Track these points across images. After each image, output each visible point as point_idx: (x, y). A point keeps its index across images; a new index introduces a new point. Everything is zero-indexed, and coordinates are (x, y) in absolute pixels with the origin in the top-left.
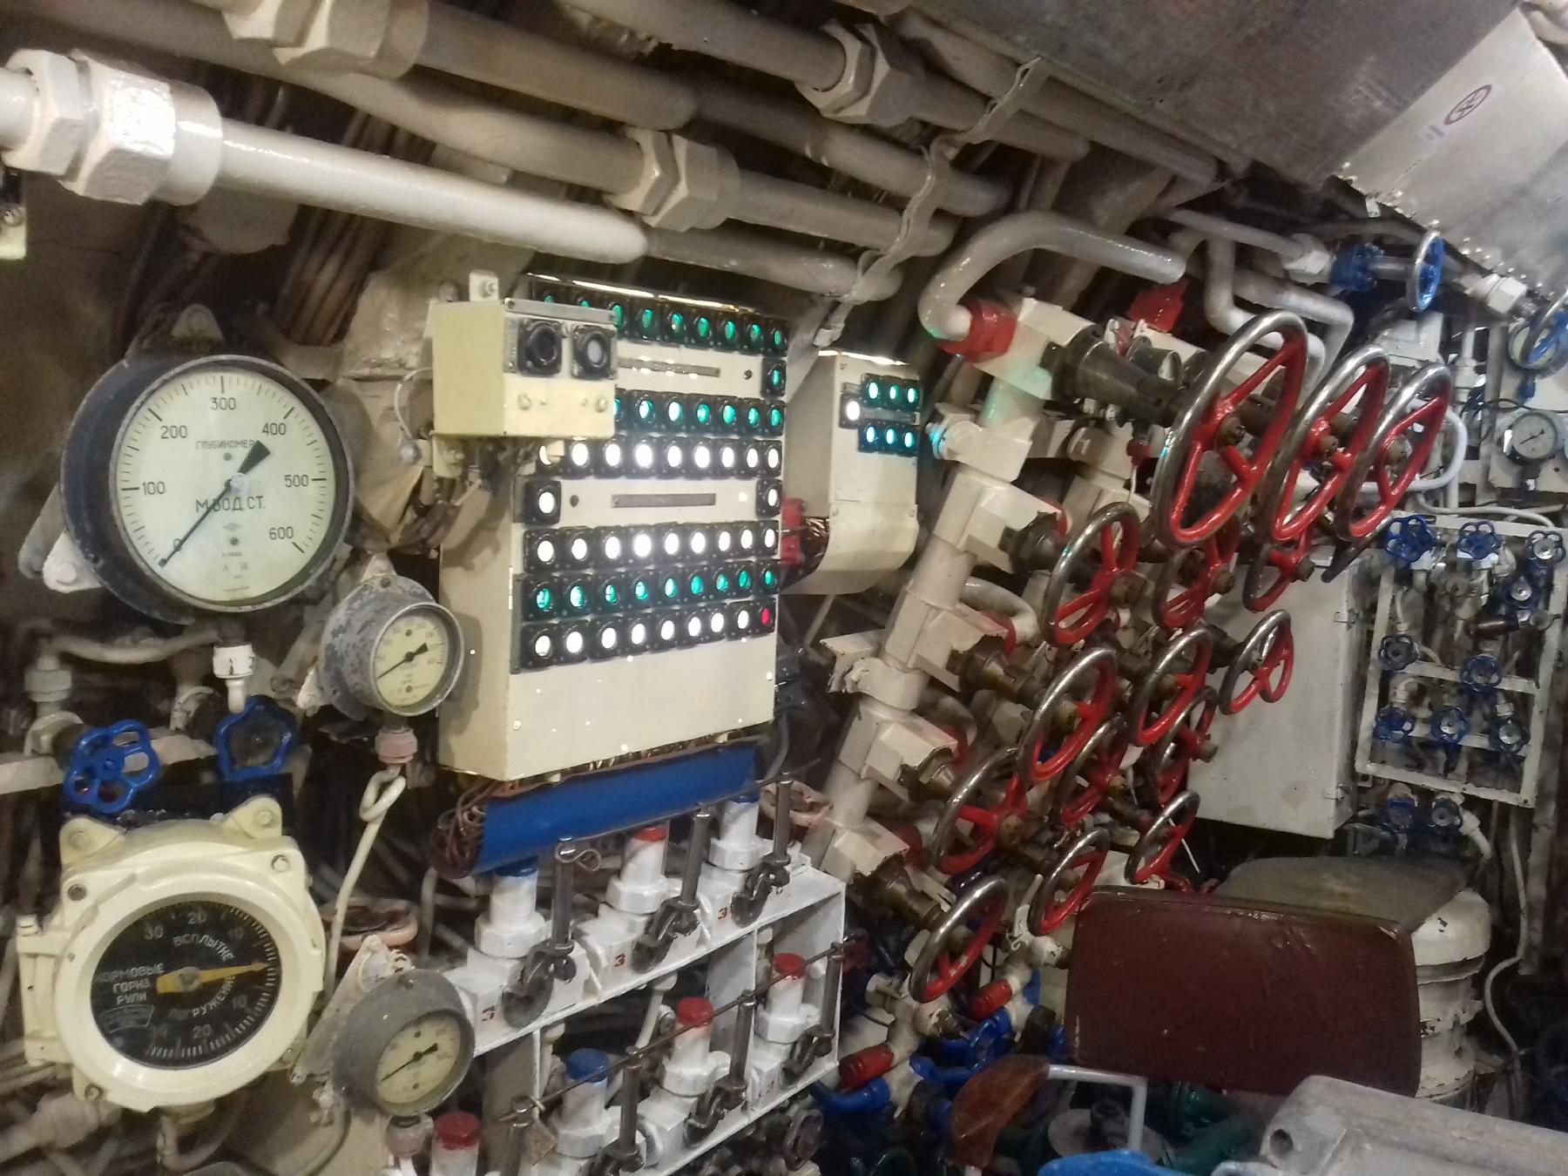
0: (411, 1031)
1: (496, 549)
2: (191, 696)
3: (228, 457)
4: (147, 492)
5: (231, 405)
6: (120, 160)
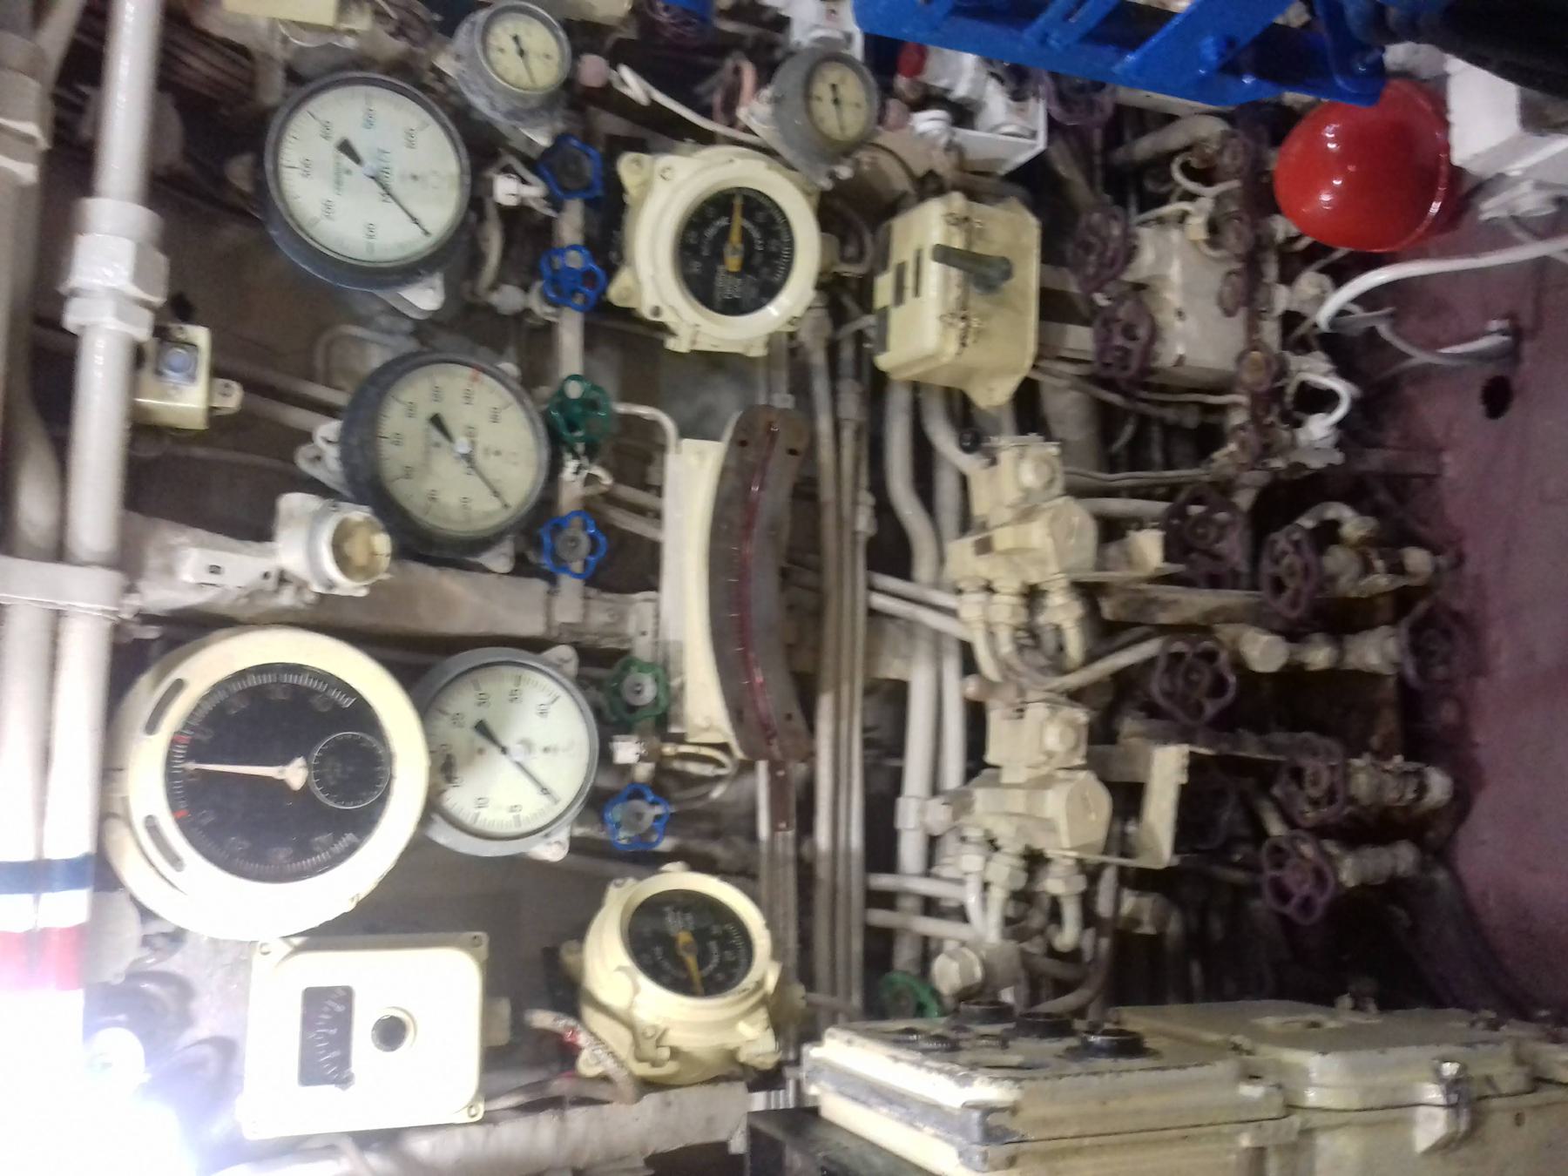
0: (815, 104)
3: (348, 172)
5: (307, 164)
6: (139, 277)
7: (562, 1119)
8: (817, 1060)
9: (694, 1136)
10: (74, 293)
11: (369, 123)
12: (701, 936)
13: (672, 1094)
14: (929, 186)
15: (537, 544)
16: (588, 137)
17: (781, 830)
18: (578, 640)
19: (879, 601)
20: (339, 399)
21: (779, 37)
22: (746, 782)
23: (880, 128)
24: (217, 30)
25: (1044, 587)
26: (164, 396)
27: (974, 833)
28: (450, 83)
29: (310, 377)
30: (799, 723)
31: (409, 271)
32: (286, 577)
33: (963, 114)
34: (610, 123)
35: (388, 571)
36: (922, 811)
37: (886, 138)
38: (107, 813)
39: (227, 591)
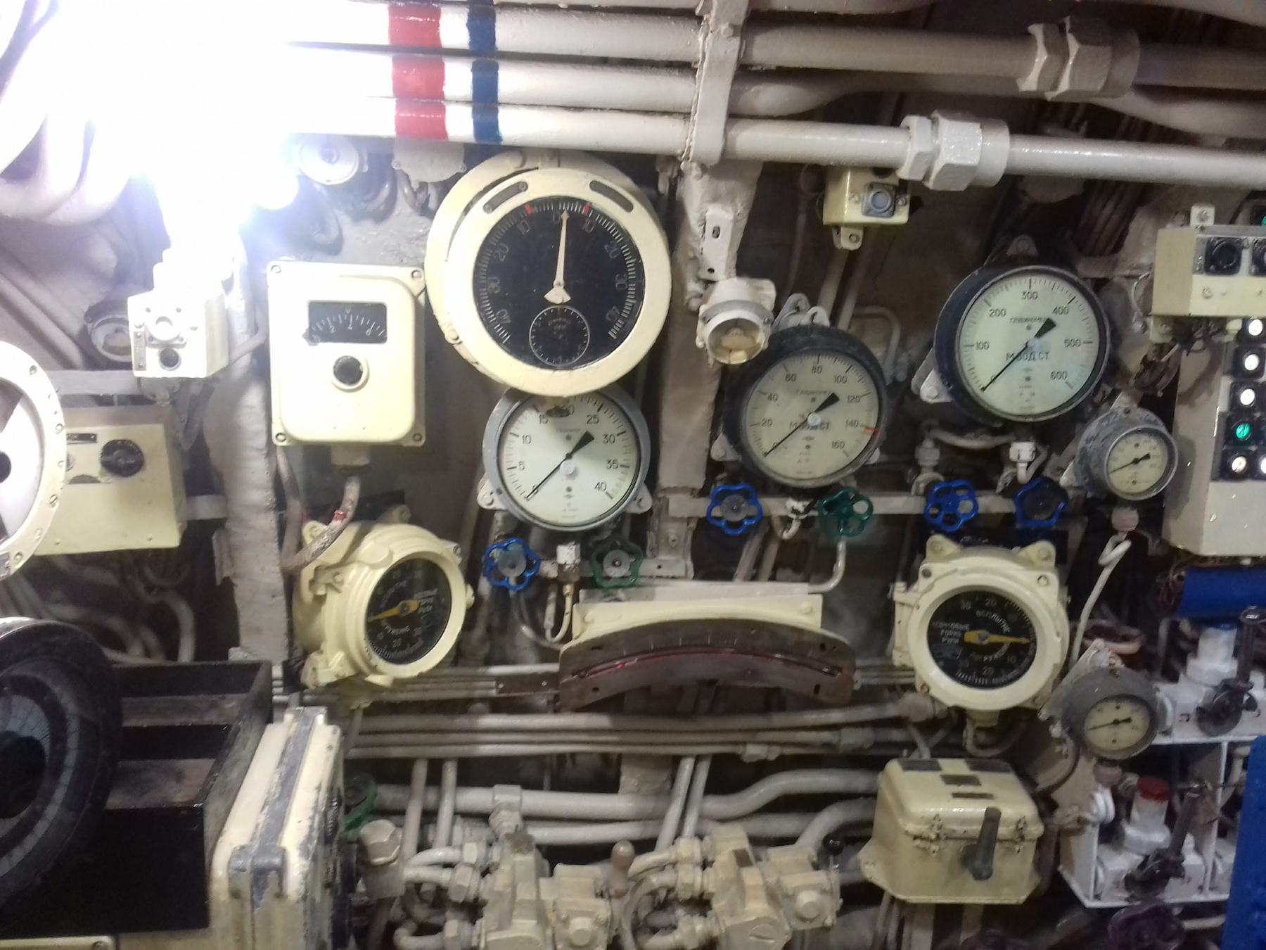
0: (1113, 704)
1: (1211, 393)
2: (1010, 474)
3: (1029, 328)
4: (978, 347)
6: (949, 168)
7: (268, 509)
8: (314, 719)
9: (246, 618)
10: (935, 122)
11: (1069, 343)
12: (412, 619)
13: (281, 599)
14: (1046, 803)
15: (733, 480)
16: (1065, 516)
17: (498, 684)
18: (654, 513)
19: (687, 766)
20: (843, 324)
21: (1157, 674)
22: (531, 655)
23: (1094, 761)
24: (1134, 227)
25: (709, 913)
26: (853, 192)
27: (495, 854)
28: (1104, 406)
29: (860, 303)
30: (592, 698)
31: (952, 376)
32: (710, 286)
33: (1110, 834)
34: (1076, 533)
35: (716, 361)
36: (509, 807)
37: (1085, 768)
38: (528, 154)
39: (699, 242)
